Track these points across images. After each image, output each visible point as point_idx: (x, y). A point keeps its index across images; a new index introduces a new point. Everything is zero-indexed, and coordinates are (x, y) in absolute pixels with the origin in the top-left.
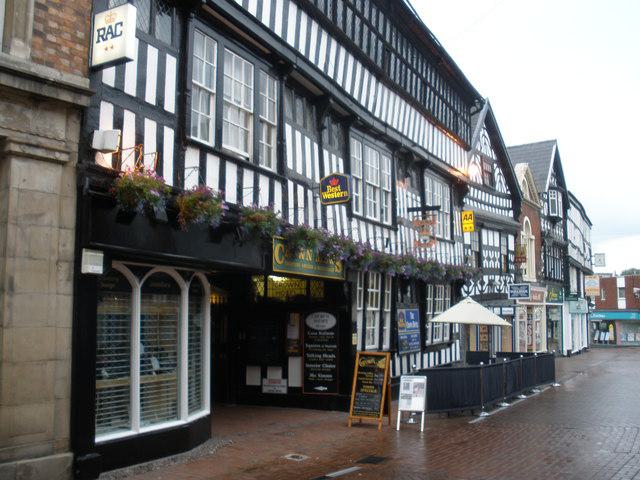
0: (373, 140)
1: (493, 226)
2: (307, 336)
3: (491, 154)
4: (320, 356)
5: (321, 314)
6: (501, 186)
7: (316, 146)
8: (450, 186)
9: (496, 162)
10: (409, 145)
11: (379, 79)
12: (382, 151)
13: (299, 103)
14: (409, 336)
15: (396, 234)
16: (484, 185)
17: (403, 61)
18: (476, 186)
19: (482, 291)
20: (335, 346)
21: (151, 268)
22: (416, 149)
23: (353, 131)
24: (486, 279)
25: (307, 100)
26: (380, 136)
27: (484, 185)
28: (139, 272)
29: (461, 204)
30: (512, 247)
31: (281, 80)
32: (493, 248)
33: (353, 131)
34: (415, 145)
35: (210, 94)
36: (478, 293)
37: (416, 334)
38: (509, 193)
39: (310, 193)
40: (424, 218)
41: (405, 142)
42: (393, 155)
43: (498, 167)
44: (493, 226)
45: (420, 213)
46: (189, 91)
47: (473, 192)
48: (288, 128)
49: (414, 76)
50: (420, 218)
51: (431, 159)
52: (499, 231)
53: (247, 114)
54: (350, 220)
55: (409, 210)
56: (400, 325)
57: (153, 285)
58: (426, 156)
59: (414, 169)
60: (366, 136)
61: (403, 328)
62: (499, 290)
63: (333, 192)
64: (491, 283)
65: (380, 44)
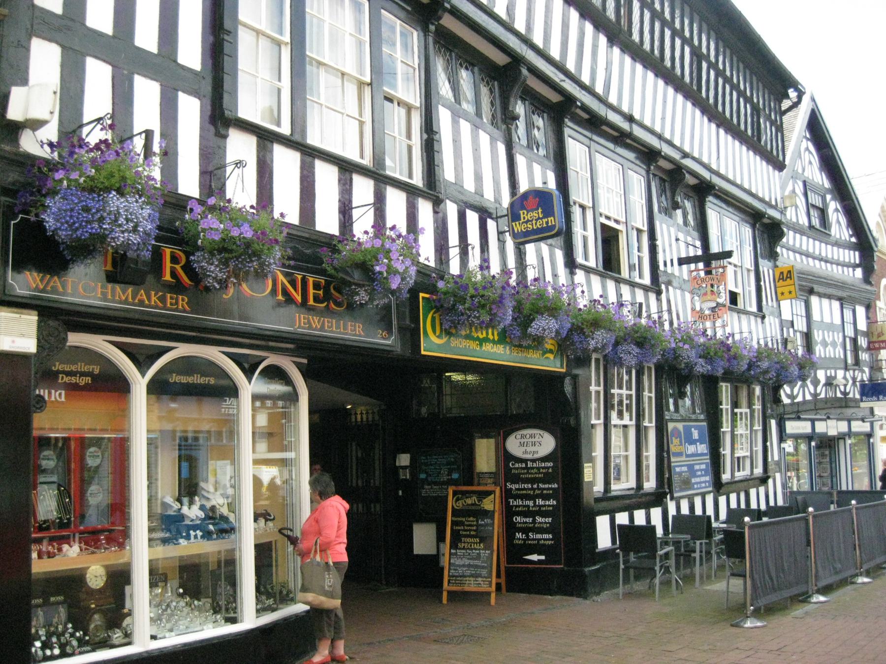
0: (611, 145)
1: (830, 291)
2: (508, 470)
3: (821, 179)
4: (531, 503)
5: (528, 432)
6: (840, 228)
7: (501, 148)
8: (753, 227)
9: (830, 191)
10: (676, 156)
11: (613, 40)
12: (627, 164)
13: (465, 76)
14: (691, 467)
15: (659, 299)
16: (811, 227)
17: (741, 94)
18: (797, 229)
19: (815, 395)
20: (556, 486)
21: (168, 349)
22: (688, 162)
23: (570, 130)
24: (821, 375)
25: (481, 70)
26: (621, 138)
27: (811, 227)
28: (142, 360)
29: (773, 256)
30: (862, 325)
31: (425, 30)
32: (830, 327)
33: (570, 130)
34: (686, 155)
35: (278, 44)
36: (808, 397)
37: (703, 464)
38: (853, 240)
39: (491, 225)
40: (709, 273)
41: (666, 150)
42: (648, 171)
43: (834, 199)
44: (830, 291)
45: (701, 265)
46: (233, 33)
47: (790, 238)
48: (444, 117)
49: (678, 42)
50: (702, 274)
51: (716, 180)
52: (840, 299)
53: (361, 84)
54: (572, 273)
55: (682, 262)
56: (673, 449)
57: (175, 378)
58: (706, 175)
59: (688, 197)
60: (595, 138)
61: (679, 454)
62: (845, 394)
63: (532, 217)
64: (829, 383)
65: (687, 50)
